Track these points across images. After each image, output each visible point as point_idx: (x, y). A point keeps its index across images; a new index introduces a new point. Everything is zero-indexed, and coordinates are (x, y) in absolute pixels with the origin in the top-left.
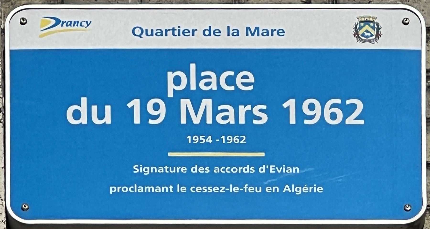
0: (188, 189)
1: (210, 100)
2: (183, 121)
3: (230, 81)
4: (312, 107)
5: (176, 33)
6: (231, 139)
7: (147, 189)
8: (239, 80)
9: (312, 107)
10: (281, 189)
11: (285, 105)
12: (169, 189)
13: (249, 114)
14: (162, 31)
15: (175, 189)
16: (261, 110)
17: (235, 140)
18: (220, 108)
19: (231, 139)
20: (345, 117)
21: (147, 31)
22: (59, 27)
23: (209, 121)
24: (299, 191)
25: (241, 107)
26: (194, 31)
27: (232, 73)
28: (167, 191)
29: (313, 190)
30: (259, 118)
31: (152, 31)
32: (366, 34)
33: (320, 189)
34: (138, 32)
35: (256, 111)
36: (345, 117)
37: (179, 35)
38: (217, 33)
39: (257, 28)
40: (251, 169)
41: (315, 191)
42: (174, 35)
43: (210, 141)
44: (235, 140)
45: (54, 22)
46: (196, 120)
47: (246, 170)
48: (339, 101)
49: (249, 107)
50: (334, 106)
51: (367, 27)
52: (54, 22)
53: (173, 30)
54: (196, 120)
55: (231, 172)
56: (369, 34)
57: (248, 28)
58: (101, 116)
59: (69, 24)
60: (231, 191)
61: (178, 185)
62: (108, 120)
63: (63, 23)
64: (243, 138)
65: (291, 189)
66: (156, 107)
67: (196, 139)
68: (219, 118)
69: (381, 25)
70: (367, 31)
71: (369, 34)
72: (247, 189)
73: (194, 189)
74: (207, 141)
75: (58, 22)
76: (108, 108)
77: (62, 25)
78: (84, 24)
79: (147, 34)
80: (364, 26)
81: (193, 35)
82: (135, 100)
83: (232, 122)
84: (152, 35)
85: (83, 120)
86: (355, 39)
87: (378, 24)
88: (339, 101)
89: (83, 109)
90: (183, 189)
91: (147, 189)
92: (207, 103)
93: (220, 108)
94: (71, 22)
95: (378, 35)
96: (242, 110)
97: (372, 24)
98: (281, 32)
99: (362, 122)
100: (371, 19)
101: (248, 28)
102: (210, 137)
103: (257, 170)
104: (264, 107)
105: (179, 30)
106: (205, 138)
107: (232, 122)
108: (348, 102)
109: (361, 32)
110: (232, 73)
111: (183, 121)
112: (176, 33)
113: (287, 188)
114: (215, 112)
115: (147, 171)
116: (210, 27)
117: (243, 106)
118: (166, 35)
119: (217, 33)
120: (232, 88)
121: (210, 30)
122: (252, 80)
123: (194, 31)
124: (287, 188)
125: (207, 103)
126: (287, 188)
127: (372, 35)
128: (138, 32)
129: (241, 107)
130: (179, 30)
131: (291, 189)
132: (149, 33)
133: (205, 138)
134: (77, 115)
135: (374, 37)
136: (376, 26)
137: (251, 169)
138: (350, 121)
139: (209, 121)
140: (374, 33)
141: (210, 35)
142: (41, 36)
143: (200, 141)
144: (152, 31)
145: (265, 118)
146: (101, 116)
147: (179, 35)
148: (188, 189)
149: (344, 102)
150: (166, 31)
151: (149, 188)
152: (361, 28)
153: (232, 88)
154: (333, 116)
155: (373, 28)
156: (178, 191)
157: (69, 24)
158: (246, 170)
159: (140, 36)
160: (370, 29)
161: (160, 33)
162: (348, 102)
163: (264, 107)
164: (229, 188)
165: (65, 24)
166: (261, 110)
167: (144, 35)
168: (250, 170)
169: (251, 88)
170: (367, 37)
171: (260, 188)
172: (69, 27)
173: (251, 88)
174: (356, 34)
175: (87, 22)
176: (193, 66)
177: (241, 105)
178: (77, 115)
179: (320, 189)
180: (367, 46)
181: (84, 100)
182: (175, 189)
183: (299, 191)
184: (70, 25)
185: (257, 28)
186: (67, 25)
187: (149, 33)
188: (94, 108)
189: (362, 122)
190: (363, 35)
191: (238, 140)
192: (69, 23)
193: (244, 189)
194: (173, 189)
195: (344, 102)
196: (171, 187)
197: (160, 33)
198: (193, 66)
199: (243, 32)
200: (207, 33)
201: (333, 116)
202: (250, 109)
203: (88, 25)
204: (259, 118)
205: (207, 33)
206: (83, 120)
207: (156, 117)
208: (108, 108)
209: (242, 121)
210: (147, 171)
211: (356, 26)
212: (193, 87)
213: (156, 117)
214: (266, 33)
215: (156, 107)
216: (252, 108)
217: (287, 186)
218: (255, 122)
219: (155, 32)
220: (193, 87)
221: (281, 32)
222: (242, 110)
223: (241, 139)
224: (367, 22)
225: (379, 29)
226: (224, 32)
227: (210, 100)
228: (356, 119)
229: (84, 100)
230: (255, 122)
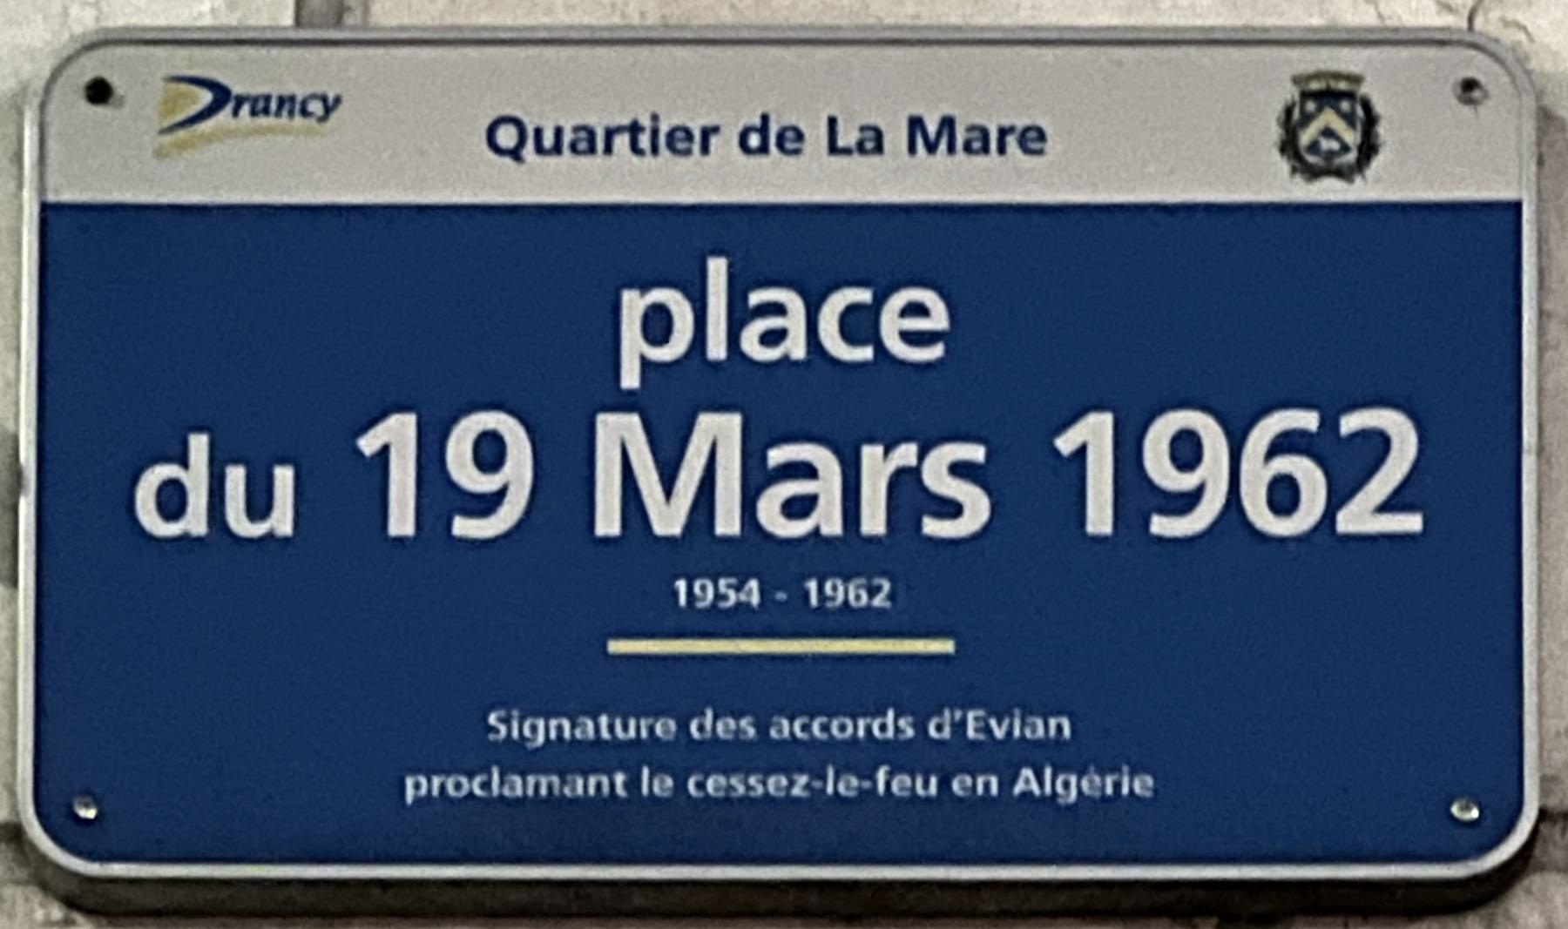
0: (681, 786)
1: (735, 420)
2: (608, 522)
4: (1186, 451)
5: (644, 141)
7: (537, 787)
8: (891, 325)
9: (1186, 451)
10: (1007, 782)
11: (1066, 444)
12: (612, 786)
13: (905, 483)
14: (591, 134)
15: (633, 784)
18: (777, 456)
20: (1338, 498)
21: (538, 133)
22: (224, 116)
24: (1071, 788)
26: (707, 133)
27: (864, 296)
28: (606, 789)
29: (1117, 786)
30: (952, 509)
31: (558, 132)
32: (1328, 144)
33: (1142, 785)
34: (507, 137)
35: (937, 479)
36: (1338, 498)
37: (655, 150)
40: (902, 723)
41: (1125, 790)
42: (635, 148)
43: (755, 600)
45: (206, 97)
46: (668, 519)
47: (883, 728)
48: (1309, 420)
49: (906, 454)
50: (1283, 444)
51: (1329, 118)
52: (206, 97)
54: (668, 519)
55: (880, 349)
56: (1335, 145)
57: (916, 124)
58: (259, 505)
59: (260, 106)
60: (830, 790)
61: (646, 772)
62: (282, 521)
63: (240, 101)
65: (1041, 784)
67: (706, 591)
68: (769, 511)
69: (1379, 107)
70: (1328, 133)
71: (1335, 145)
72: (888, 785)
73: (701, 786)
74: (743, 597)
75: (222, 96)
77: (236, 113)
78: (316, 107)
79: (539, 149)
80: (1320, 109)
81: (705, 149)
82: (394, 420)
84: (557, 149)
85: (195, 522)
86: (1284, 166)
87: (1367, 106)
88: (1309, 420)
90: (663, 786)
91: (537, 787)
94: (268, 98)
95: (1368, 149)
96: (876, 465)
97: (1345, 105)
99: (1411, 523)
100: (1343, 86)
102: (753, 584)
103: (921, 728)
104: (976, 453)
105: (655, 133)
106: (738, 588)
108: (1350, 423)
109: (1305, 137)
110: (864, 296)
111: (608, 522)
112: (644, 141)
113: (1026, 781)
114: (756, 480)
116: (765, 118)
117: (879, 450)
118: (608, 149)
119: (790, 141)
120: (866, 353)
121: (763, 130)
124: (1027, 781)
126: (1026, 781)
127: (1345, 148)
128: (507, 137)
129: (871, 454)
130: (655, 133)
131: (1041, 784)
132: (548, 140)
133: (738, 588)
134: (172, 501)
135: (1351, 157)
136: (1360, 112)
137: (902, 723)
138: (1358, 518)
139: (728, 522)
140: (1352, 137)
141: (763, 149)
142: (160, 154)
143: (719, 597)
144: (558, 132)
145: (977, 508)
146: (259, 505)
147: (655, 150)
148: (681, 786)
149: (1329, 423)
150: (610, 134)
151: (544, 781)
152: (1307, 119)
153: (866, 353)
155: (1349, 119)
156: (645, 790)
157: (260, 106)
158: (883, 728)
159: (515, 154)
160: (1339, 125)
161: (587, 142)
162: (1350, 423)
163: (976, 453)
164: (824, 778)
165: (246, 109)
167: (529, 150)
168: (897, 730)
169: (935, 352)
170: (1331, 154)
171: (933, 781)
172: (263, 121)
173: (935, 352)
174: (1289, 146)
175: (324, 99)
177: (872, 440)
178: (172, 501)
179: (1142, 785)
180: (1330, 191)
182: (633, 784)
183: (1071, 788)
184: (266, 111)
186: (254, 113)
187: (548, 140)
189: (1411, 523)
190: (1314, 147)
192: (261, 105)
193: (875, 783)
194: (626, 785)
195: (1329, 423)
196: (620, 779)
197: (587, 142)
200: (754, 140)
201: (1284, 495)
202: (913, 461)
203: (328, 110)
204: (952, 509)
205: (754, 140)
206: (195, 522)
207: (487, 504)
209: (874, 522)
211: (1288, 111)
213: (487, 504)
215: (490, 452)
216: (922, 456)
217: (1027, 773)
218: (933, 527)
219: (567, 138)
222: (876, 465)
223: (873, 591)
224: (1328, 97)
225: (1371, 120)
227: (735, 420)
228: (1386, 507)
230: (933, 527)
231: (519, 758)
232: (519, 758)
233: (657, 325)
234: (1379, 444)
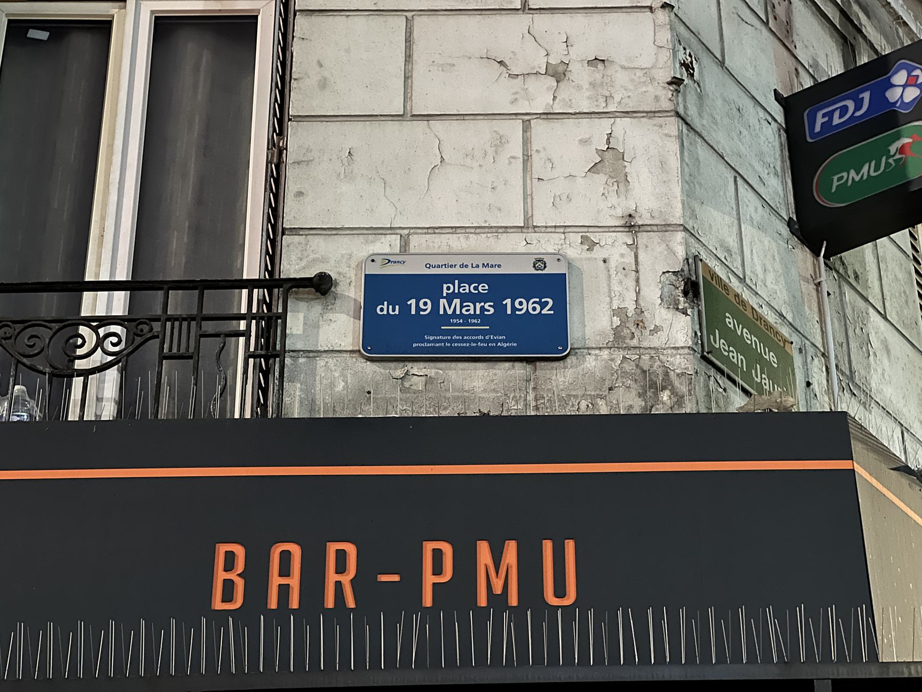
1: (459, 300)
2: (442, 312)
3: (476, 288)
6: (473, 321)
8: (480, 288)
9: (521, 304)
10: (497, 344)
16: (489, 306)
17: (475, 321)
19: (473, 321)
23: (458, 312)
25: (477, 304)
26: (455, 265)
27: (477, 285)
30: (489, 311)
35: (486, 306)
36: (541, 310)
38: (466, 266)
39: (488, 264)
44: (475, 321)
45: (387, 261)
46: (450, 312)
48: (538, 300)
51: (539, 263)
52: (387, 261)
53: (445, 265)
54: (450, 312)
57: (483, 264)
58: (394, 310)
59: (395, 262)
62: (397, 312)
64: (547, 303)
66: (425, 304)
67: (455, 321)
75: (389, 261)
76: (397, 307)
83: (473, 313)
85: (385, 312)
86: (534, 269)
88: (538, 300)
89: (385, 307)
92: (457, 301)
93: (464, 304)
95: (545, 267)
98: (499, 266)
99: (552, 312)
101: (483, 264)
104: (492, 304)
107: (473, 313)
108: (543, 300)
110: (477, 285)
111: (442, 312)
113: (499, 344)
114: (462, 307)
115: (432, 338)
119: (466, 266)
120: (477, 292)
122: (487, 287)
123: (455, 265)
125: (457, 301)
128: (428, 266)
138: (544, 312)
139: (458, 312)
140: (543, 266)
145: (492, 311)
146: (394, 310)
153: (477, 292)
154: (534, 309)
155: (542, 263)
157: (395, 262)
159: (429, 268)
161: (439, 266)
162: (543, 300)
163: (492, 304)
166: (489, 306)
169: (486, 291)
173: (486, 291)
174: (534, 266)
176: (457, 282)
178: (382, 310)
179: (515, 345)
181: (386, 303)
185: (488, 264)
188: (391, 307)
189: (552, 312)
191: (538, 307)
195: (540, 300)
197: (439, 266)
198: (457, 282)
199: (481, 266)
201: (534, 309)
204: (489, 311)
206: (385, 312)
208: (397, 307)
209: (478, 312)
210: (432, 338)
212: (456, 291)
214: (492, 266)
215: (425, 304)
220: (456, 291)
221: (499, 266)
222: (478, 306)
223: (543, 305)
224: (539, 261)
225: (545, 264)
226: (470, 266)
227: (459, 300)
229: (386, 303)
231: (429, 341)
232: (429, 341)
233: (448, 288)
234: (547, 303)
